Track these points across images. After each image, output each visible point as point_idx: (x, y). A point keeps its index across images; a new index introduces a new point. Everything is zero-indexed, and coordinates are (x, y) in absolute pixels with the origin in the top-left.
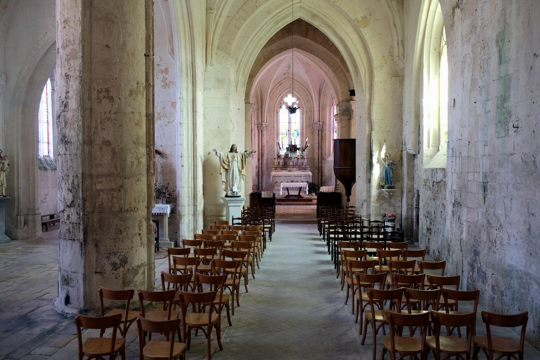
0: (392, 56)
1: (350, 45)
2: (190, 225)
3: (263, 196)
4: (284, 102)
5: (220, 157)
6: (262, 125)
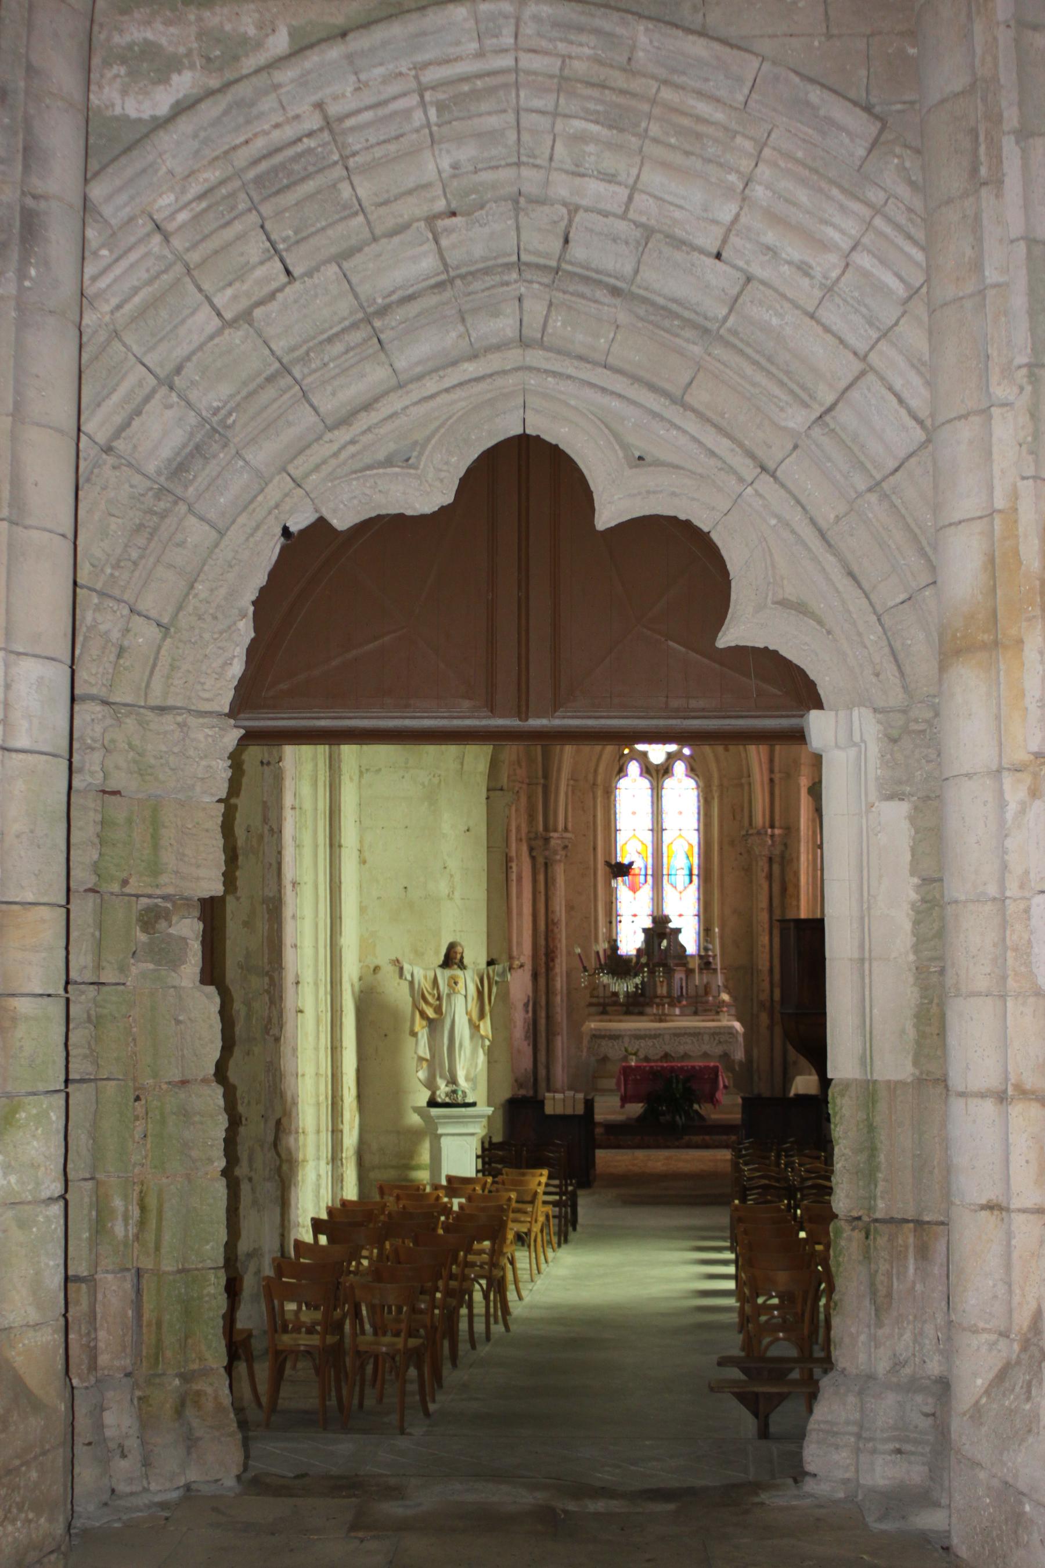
2: (323, 1191)
3: (549, 1110)
5: (412, 983)
6: (547, 840)
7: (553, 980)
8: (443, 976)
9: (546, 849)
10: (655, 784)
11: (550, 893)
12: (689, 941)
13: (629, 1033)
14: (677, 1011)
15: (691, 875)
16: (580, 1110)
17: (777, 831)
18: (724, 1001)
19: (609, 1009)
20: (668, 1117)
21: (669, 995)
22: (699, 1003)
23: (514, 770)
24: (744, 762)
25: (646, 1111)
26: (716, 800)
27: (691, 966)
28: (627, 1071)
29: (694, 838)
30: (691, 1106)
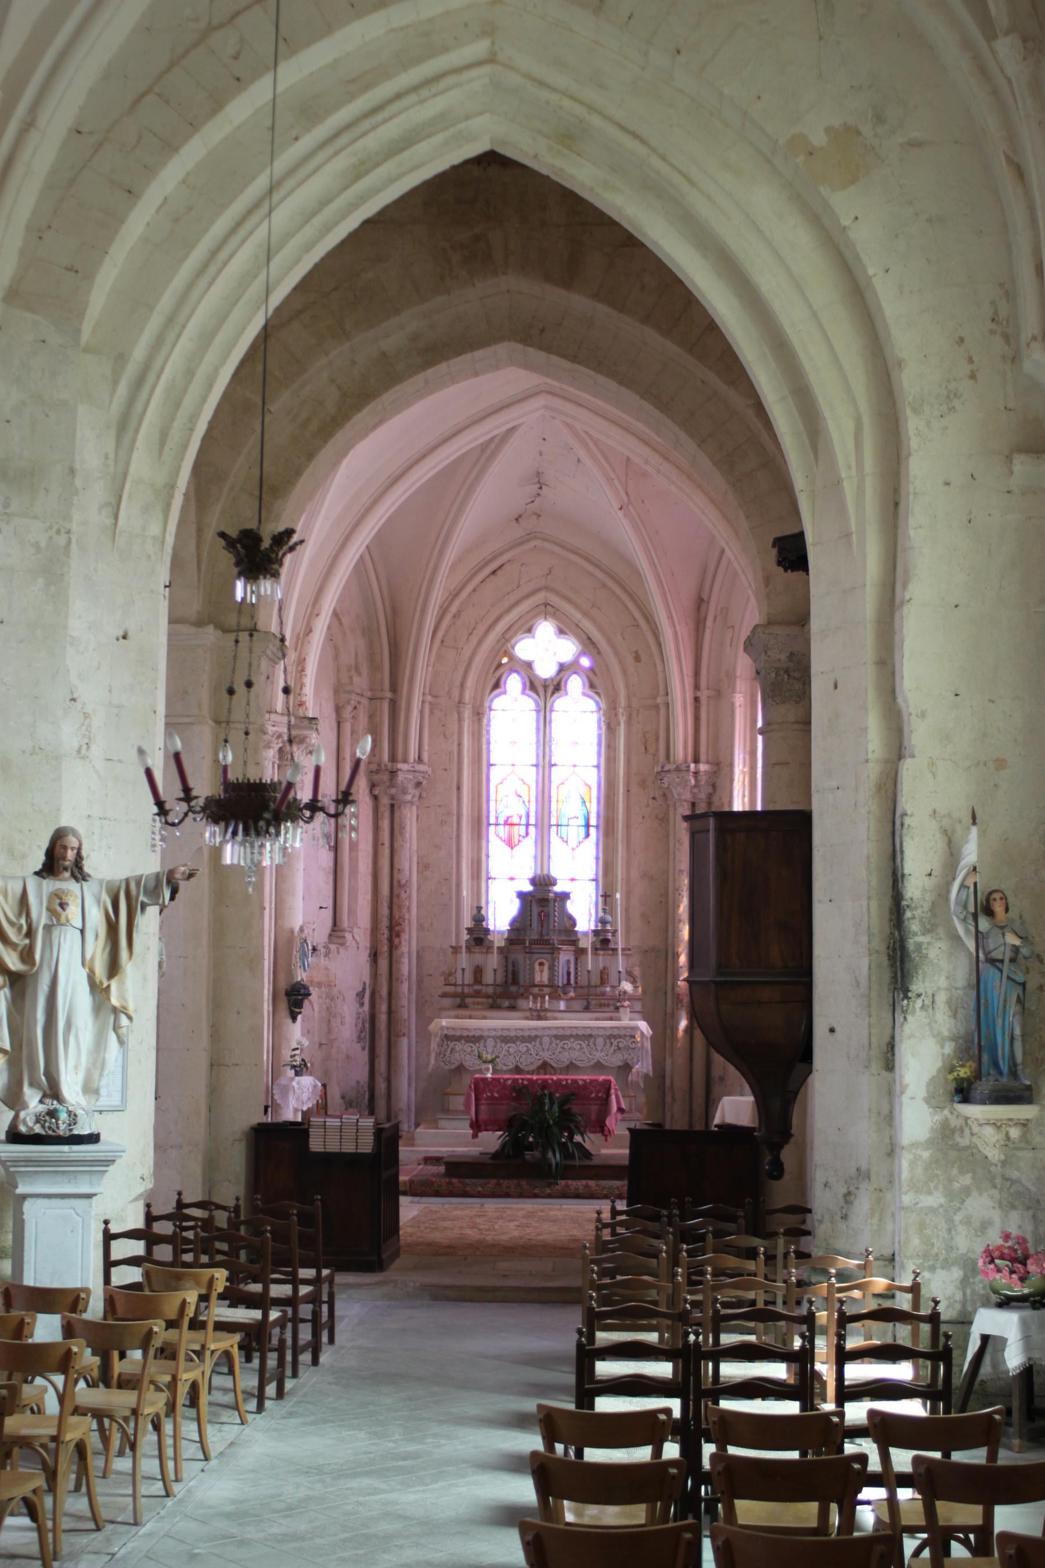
0: (1006, 337)
1: (770, 283)
4: (512, 658)
6: (393, 773)
7: (398, 962)
8: (39, 892)
9: (392, 786)
10: (542, 704)
11: (396, 845)
12: (583, 911)
13: (493, 1033)
14: (562, 1005)
15: (588, 826)
16: (367, 1145)
17: (703, 767)
18: (625, 992)
19: (469, 1001)
20: (537, 1154)
21: (552, 985)
22: (594, 997)
23: (351, 678)
24: (661, 676)
25: (504, 1146)
26: (622, 726)
27: (582, 944)
28: (480, 1086)
29: (592, 777)
30: (571, 1137)
